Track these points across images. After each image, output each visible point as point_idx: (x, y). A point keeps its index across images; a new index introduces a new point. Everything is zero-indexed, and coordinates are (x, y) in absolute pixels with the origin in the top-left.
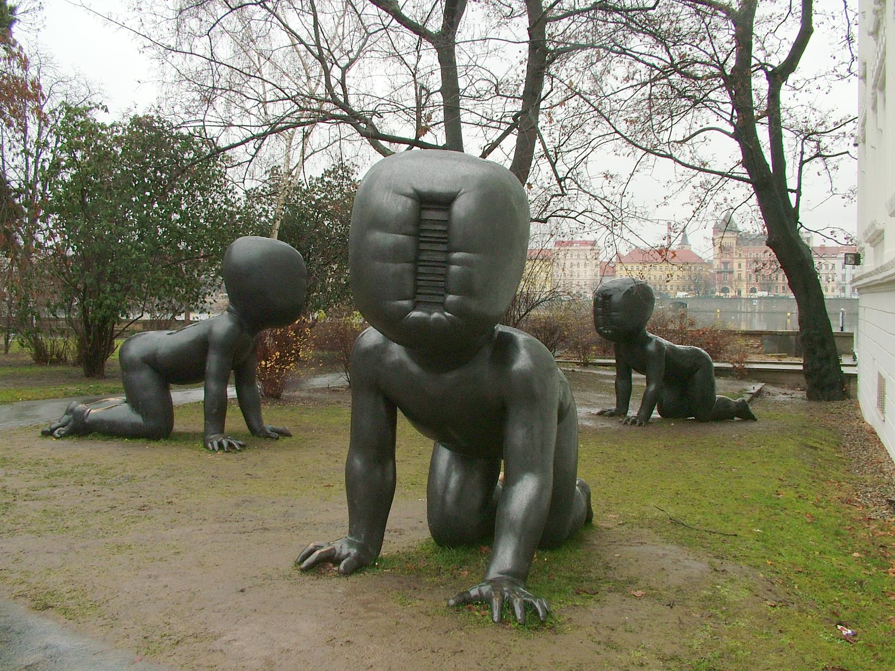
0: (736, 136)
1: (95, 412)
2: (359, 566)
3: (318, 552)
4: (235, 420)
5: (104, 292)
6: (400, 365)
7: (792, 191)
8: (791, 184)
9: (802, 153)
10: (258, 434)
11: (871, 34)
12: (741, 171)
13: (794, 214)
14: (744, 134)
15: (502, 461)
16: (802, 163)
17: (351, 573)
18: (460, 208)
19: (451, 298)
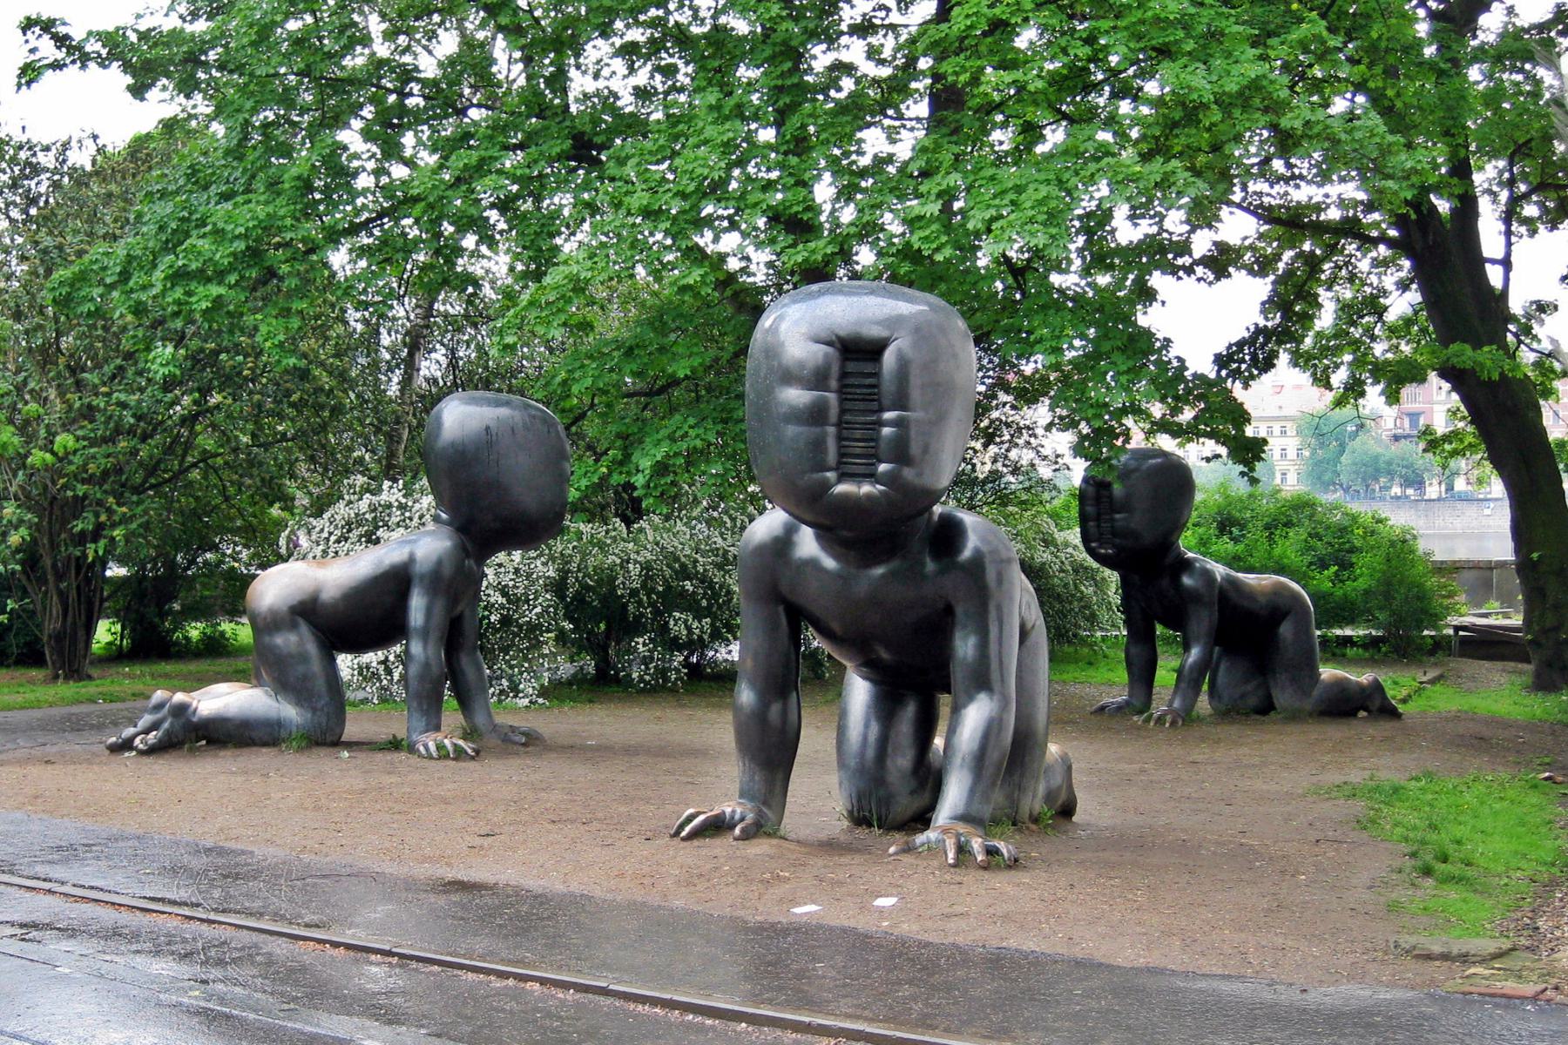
2: (756, 830)
6: (813, 563)
7: (1494, 262)
18: (889, 358)
19: (883, 467)
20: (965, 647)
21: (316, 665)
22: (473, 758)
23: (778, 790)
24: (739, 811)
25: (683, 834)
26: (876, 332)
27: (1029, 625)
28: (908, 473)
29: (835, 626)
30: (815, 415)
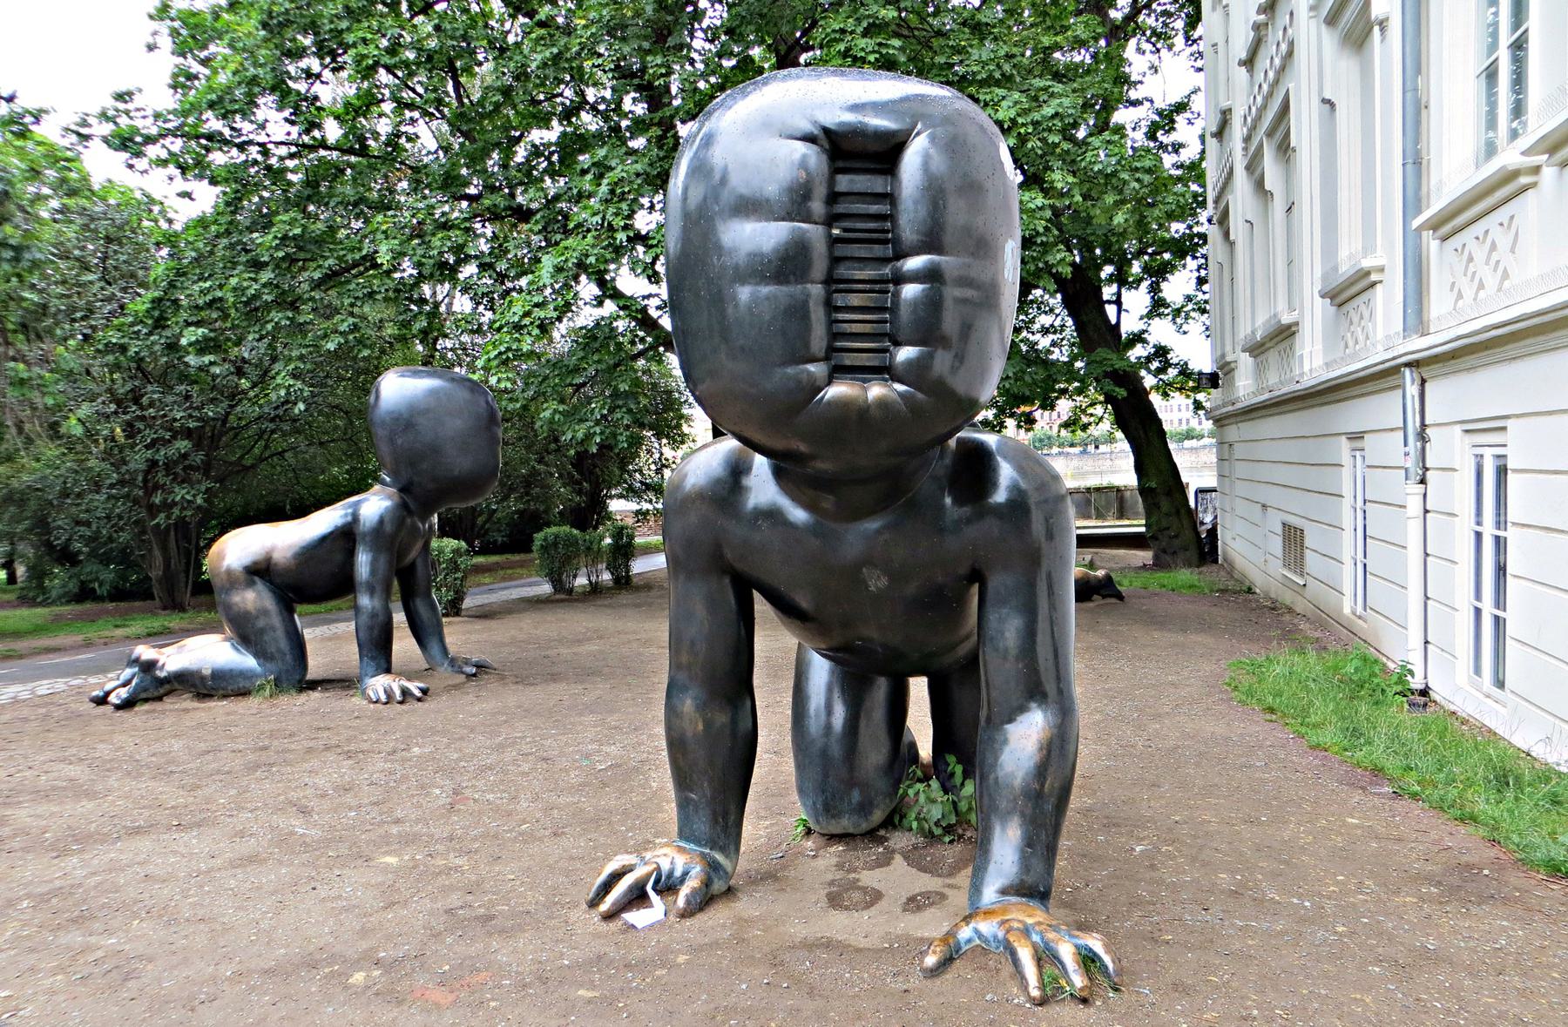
4: (404, 645)
5: (448, 746)
6: (772, 515)
7: (1109, 302)
11: (1242, 63)
19: (905, 353)
21: (276, 620)
22: (419, 700)
23: (733, 830)
28: (942, 362)
29: (804, 602)
30: (787, 265)
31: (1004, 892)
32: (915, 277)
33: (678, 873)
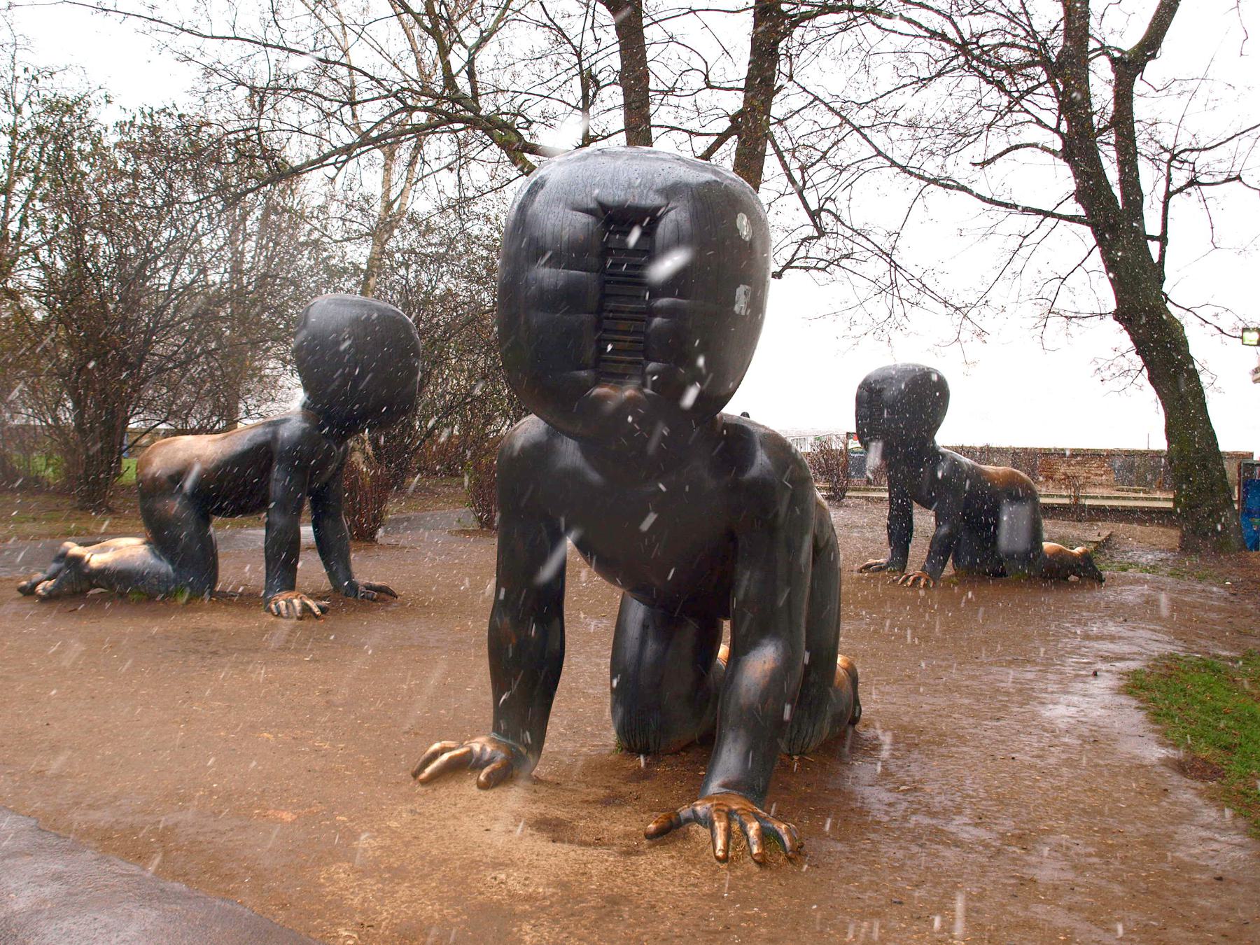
0: (1067, 154)
1: (97, 558)
3: (445, 757)
4: (310, 567)
7: (1153, 238)
8: (1152, 225)
9: (1169, 180)
10: (349, 598)
12: (1073, 208)
13: (1157, 272)
14: (1078, 149)
15: (727, 625)
16: (1168, 195)
17: (496, 785)
20: (747, 582)
24: (489, 749)
25: (423, 776)
26: (653, 200)
27: (822, 544)
30: (568, 297)
31: (724, 786)
32: (662, 312)
33: (486, 757)
